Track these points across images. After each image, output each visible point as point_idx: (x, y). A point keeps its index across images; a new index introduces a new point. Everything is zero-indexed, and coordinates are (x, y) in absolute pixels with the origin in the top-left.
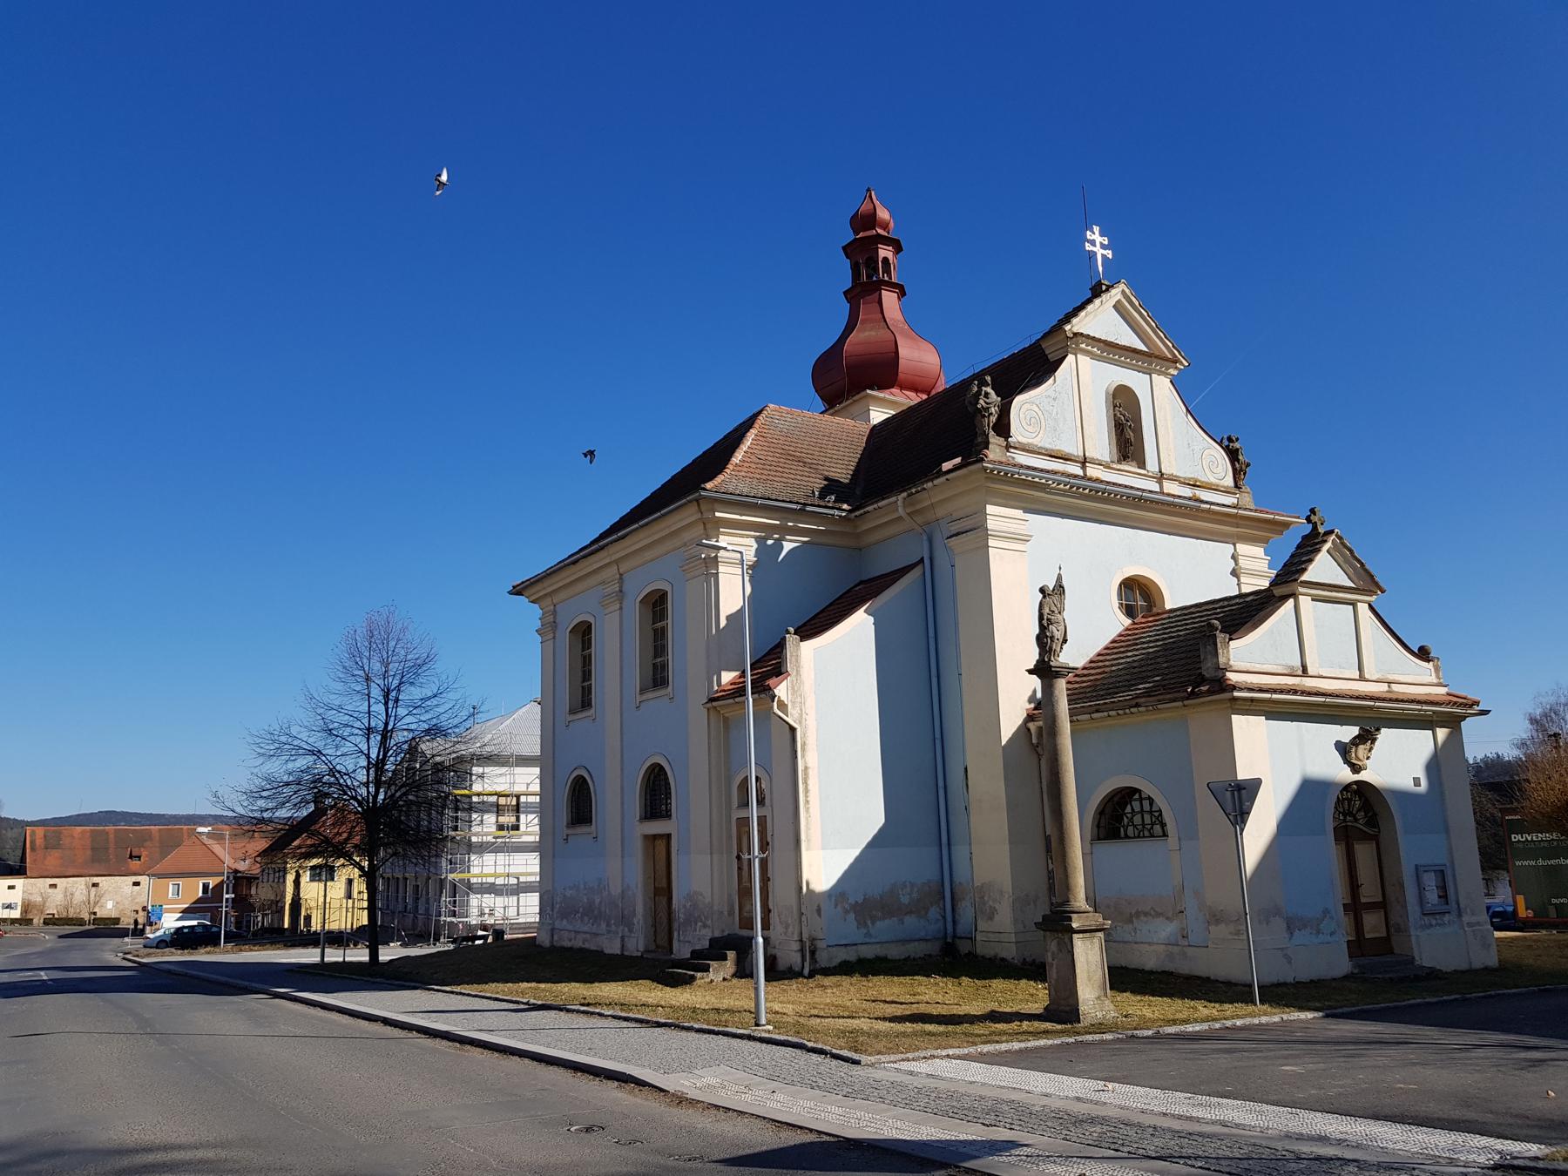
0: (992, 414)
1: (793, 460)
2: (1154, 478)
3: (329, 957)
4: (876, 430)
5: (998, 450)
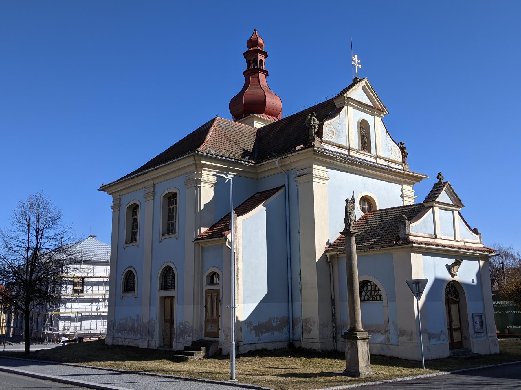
0: (316, 128)
1: (229, 141)
2: (374, 157)
4: (259, 130)
5: (318, 143)
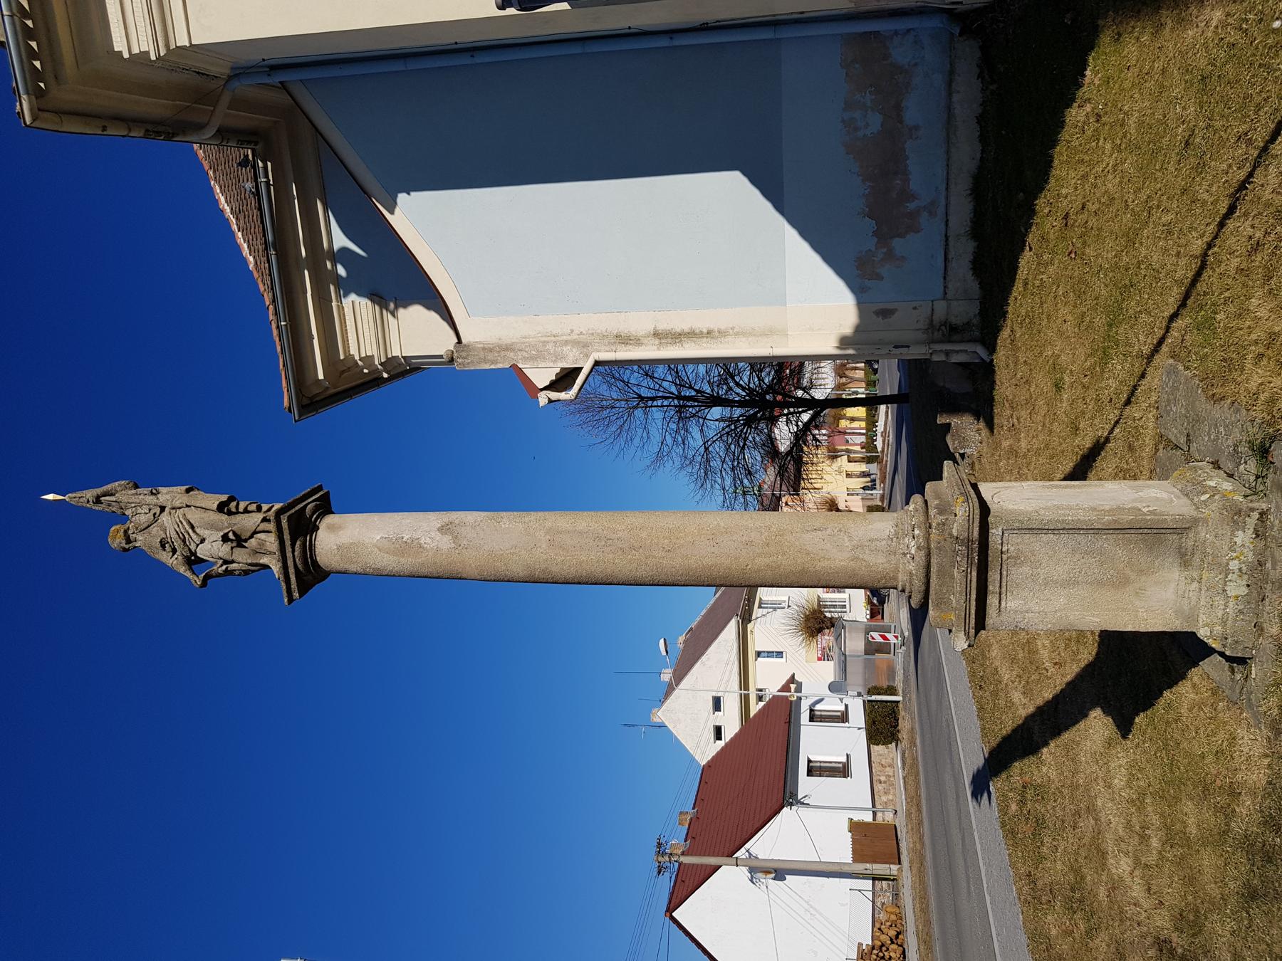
3: (892, 407)
